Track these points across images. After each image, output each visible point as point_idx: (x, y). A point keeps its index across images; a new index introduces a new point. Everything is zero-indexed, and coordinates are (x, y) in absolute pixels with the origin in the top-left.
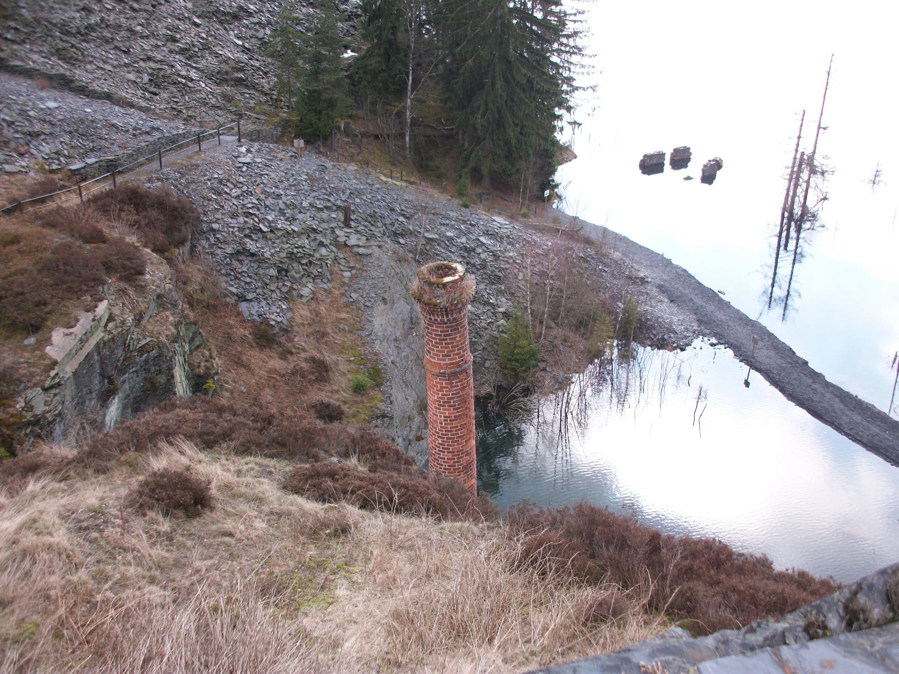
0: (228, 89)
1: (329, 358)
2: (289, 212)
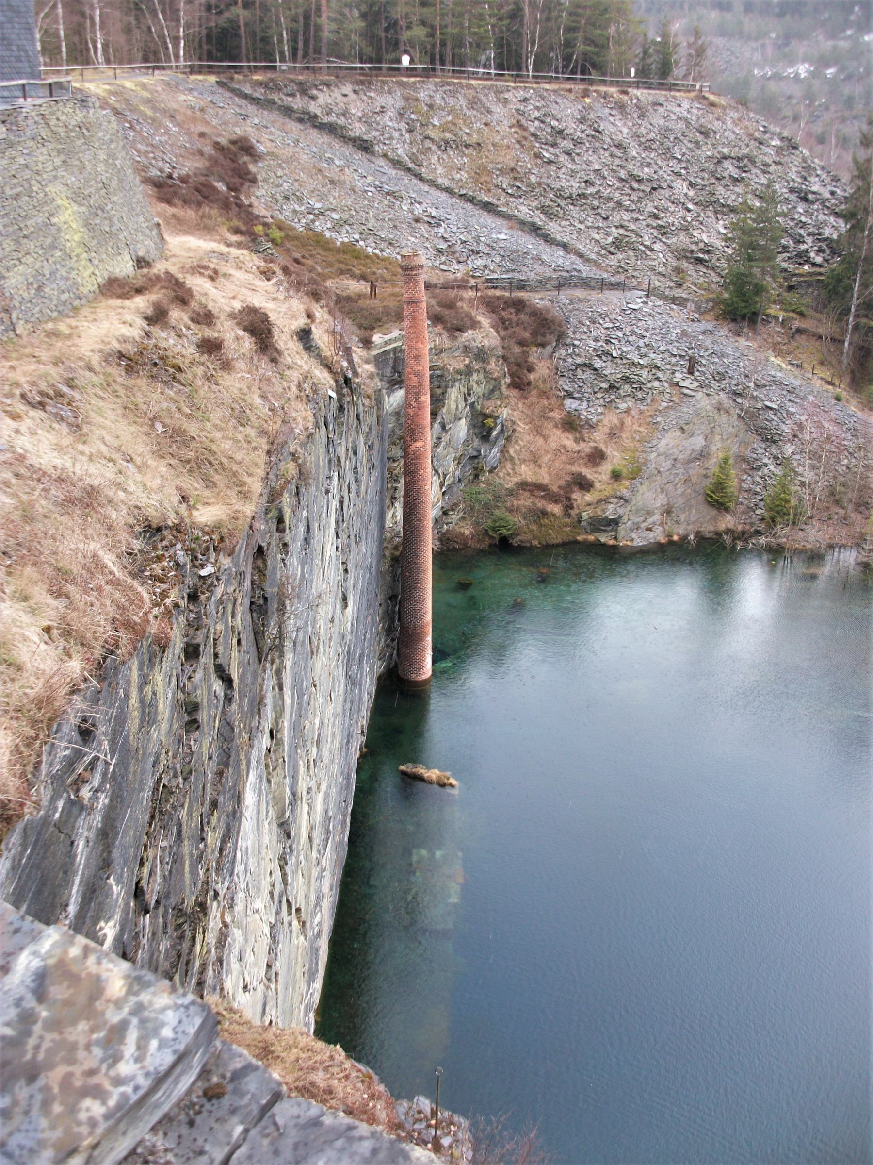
0: (685, 265)
1: (608, 451)
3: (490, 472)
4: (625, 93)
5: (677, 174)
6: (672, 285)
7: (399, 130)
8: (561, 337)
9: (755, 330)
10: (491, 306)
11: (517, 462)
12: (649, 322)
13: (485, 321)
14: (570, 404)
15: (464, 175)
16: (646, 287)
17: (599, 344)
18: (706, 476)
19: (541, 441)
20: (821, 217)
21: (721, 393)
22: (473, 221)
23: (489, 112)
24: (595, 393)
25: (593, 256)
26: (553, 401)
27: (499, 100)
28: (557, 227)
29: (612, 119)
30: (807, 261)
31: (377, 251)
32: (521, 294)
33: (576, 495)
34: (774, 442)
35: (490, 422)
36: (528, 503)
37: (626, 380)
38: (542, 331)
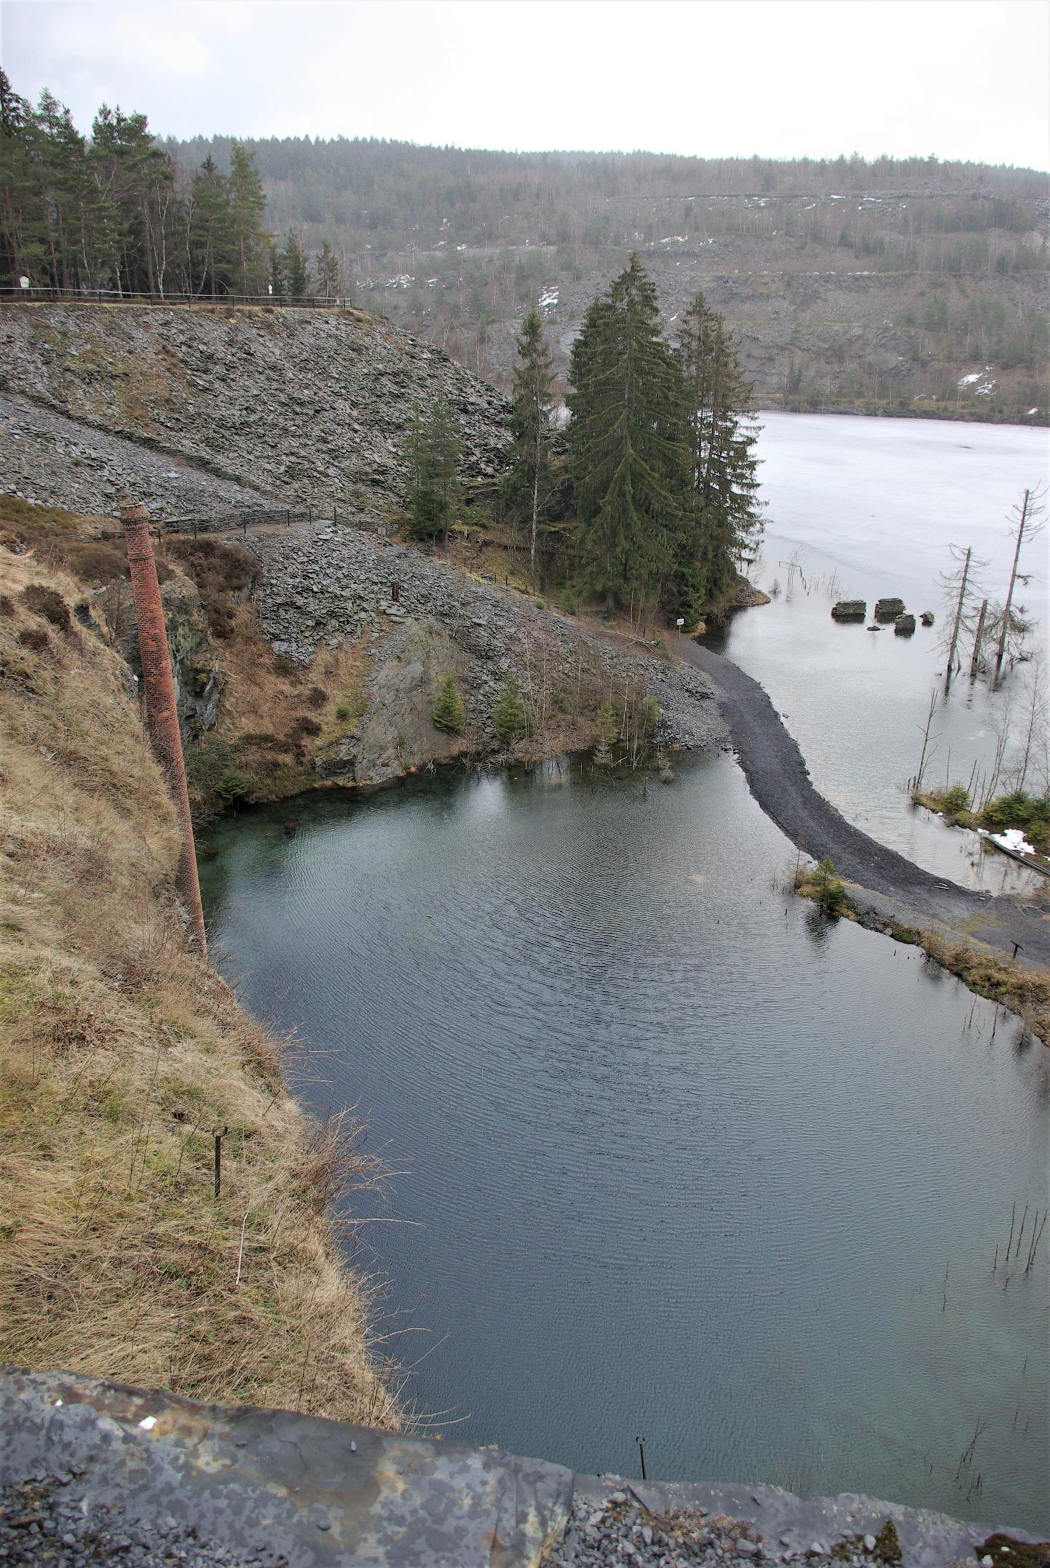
0: (362, 488)
1: (328, 691)
2: (345, 581)
3: (209, 730)
4: (270, 311)
5: (338, 394)
6: (354, 510)
7: (34, 362)
8: (256, 578)
9: (443, 548)
10: (180, 552)
11: (236, 715)
12: (344, 552)
13: (178, 569)
14: (278, 647)
15: (114, 410)
16: (331, 514)
17: (298, 580)
18: (430, 702)
19: (256, 690)
20: (484, 428)
21: (429, 616)
22: (137, 460)
23: (132, 338)
24: (302, 632)
25: (269, 488)
26: (260, 646)
27: (138, 324)
28: (225, 459)
29: (261, 340)
30: (480, 473)
31: (39, 502)
32: (206, 536)
33: (306, 741)
34: (489, 658)
35: (203, 677)
36: (257, 757)
37: (332, 614)
38: (236, 572)
